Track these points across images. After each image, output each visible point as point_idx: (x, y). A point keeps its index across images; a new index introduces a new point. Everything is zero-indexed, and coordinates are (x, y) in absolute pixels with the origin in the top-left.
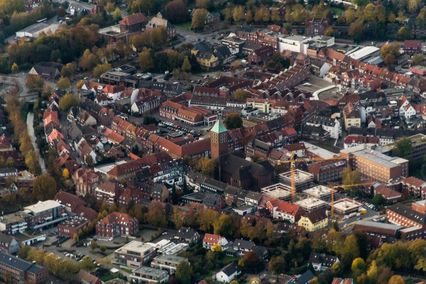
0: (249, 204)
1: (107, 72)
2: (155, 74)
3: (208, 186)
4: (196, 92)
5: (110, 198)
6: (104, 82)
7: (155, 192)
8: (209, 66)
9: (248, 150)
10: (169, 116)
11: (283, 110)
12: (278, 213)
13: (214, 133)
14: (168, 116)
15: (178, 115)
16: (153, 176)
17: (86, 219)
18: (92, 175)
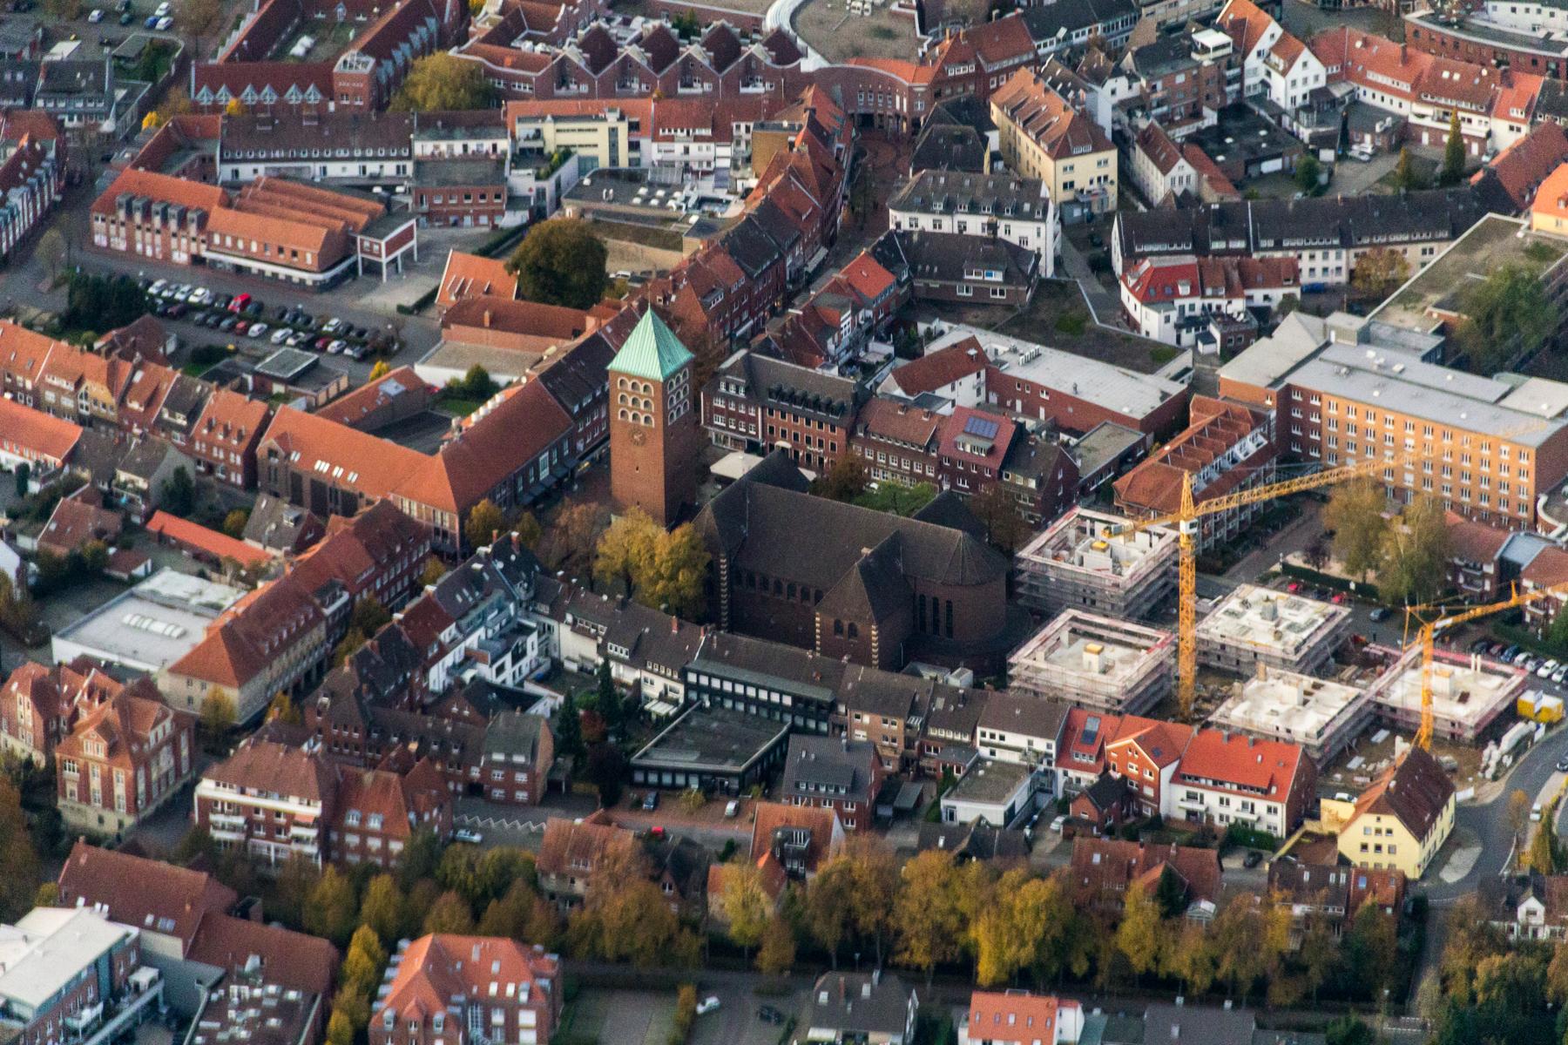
0: (1014, 758)
5: (295, 831)
7: (499, 757)
9: (719, 411)
11: (704, 145)
12: (1181, 791)
13: (630, 376)
17: (292, 995)
18: (146, 714)
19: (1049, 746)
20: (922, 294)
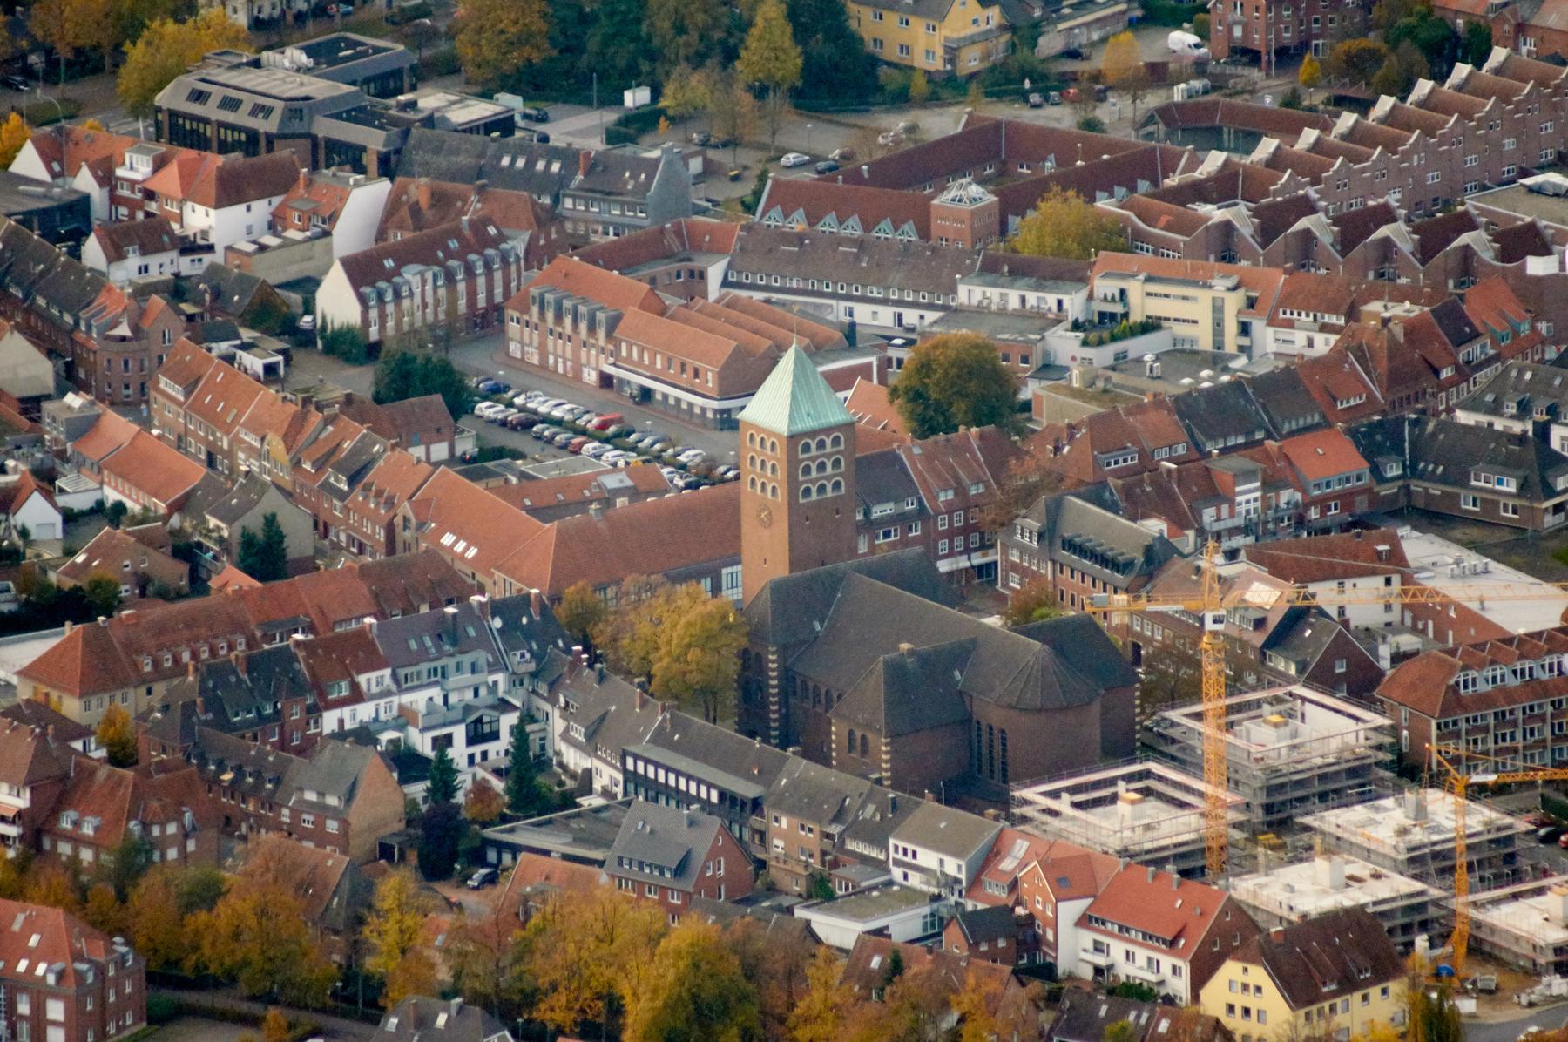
0: (915, 880)
1: (204, 73)
2: (552, 110)
3: (657, 765)
4: (776, 212)
6: (181, 133)
7: (311, 796)
8: (937, 64)
10: (554, 361)
12: (1087, 938)
13: (760, 429)
14: (560, 355)
15: (615, 354)
16: (322, 694)
19: (959, 867)
20: (1420, 503)
